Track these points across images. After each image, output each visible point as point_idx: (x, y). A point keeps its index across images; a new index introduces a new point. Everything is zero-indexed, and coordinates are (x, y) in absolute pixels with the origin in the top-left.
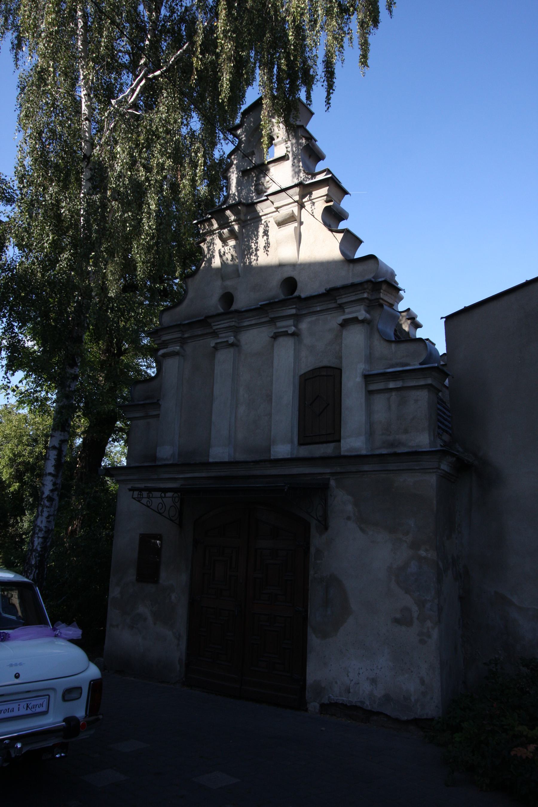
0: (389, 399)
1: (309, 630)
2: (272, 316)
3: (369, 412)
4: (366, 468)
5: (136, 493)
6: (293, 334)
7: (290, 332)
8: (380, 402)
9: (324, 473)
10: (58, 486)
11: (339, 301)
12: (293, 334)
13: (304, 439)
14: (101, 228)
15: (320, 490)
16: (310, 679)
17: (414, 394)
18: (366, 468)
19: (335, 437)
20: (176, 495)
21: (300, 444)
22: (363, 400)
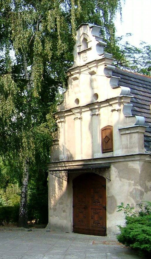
0: (127, 137)
1: (107, 212)
2: (91, 108)
3: (121, 141)
4: (120, 160)
5: (51, 172)
6: (80, 119)
7: (96, 114)
8: (124, 138)
9: (87, 164)
10: (28, 170)
11: (110, 103)
12: (80, 119)
13: (104, 151)
14: (70, 61)
15: (107, 168)
16: (107, 227)
17: (134, 135)
18: (120, 160)
19: (111, 150)
20: (65, 172)
21: (103, 153)
22: (119, 137)
